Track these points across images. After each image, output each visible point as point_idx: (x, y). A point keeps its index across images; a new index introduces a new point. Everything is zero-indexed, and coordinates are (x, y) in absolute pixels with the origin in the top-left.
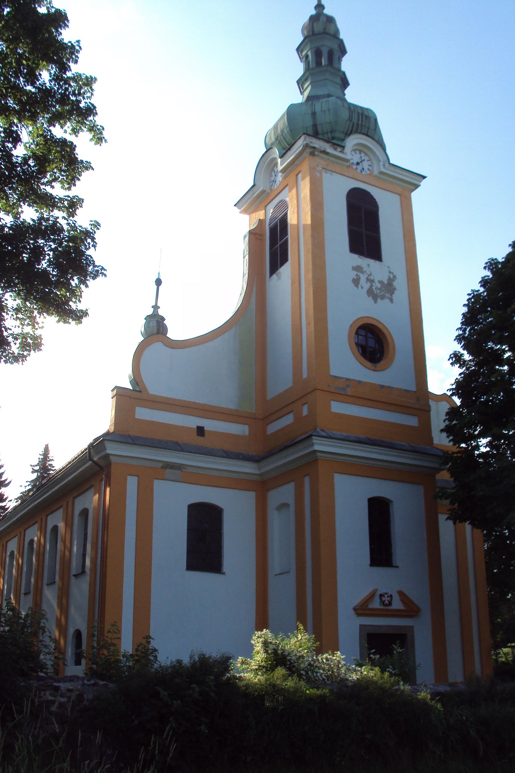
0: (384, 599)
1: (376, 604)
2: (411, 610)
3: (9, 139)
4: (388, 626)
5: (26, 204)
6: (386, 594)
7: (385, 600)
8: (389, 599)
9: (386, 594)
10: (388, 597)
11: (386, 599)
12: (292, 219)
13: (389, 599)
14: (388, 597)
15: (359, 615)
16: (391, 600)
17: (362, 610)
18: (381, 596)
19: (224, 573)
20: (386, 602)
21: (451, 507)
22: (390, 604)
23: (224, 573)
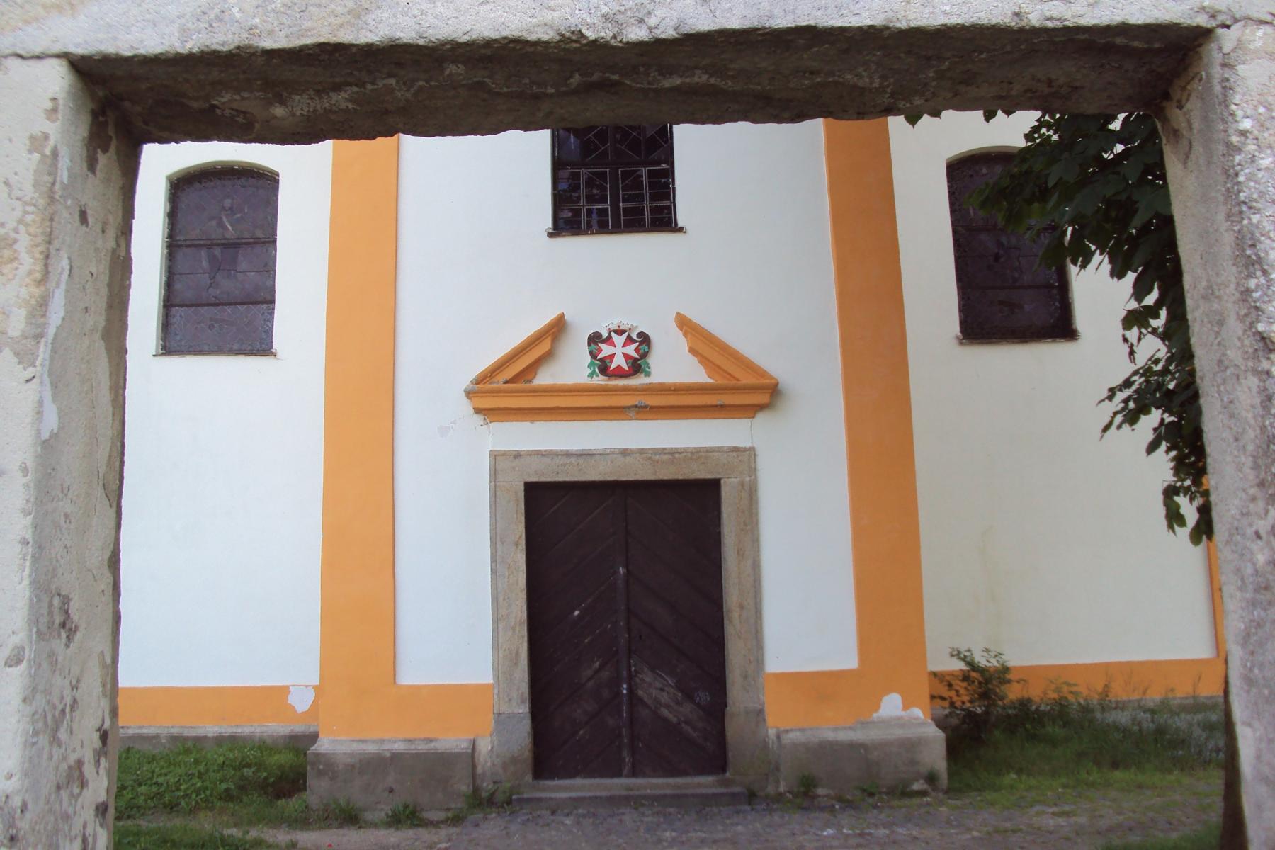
0: (606, 350)
1: (572, 367)
2: (743, 390)
3: (1168, 260)
4: (625, 453)
5: (1173, 453)
6: (620, 332)
7: (612, 357)
8: (631, 350)
9: (620, 332)
10: (630, 340)
11: (619, 353)
12: (1180, 166)
13: (631, 350)
14: (630, 340)
15: (489, 414)
16: (644, 355)
17: (509, 387)
18: (595, 339)
19: (681, 230)
20: (619, 361)
21: (1133, 305)
22: (636, 366)
23: (681, 230)
